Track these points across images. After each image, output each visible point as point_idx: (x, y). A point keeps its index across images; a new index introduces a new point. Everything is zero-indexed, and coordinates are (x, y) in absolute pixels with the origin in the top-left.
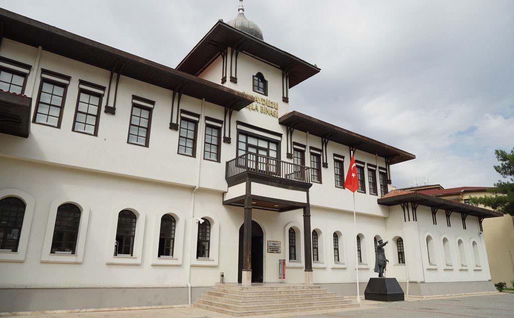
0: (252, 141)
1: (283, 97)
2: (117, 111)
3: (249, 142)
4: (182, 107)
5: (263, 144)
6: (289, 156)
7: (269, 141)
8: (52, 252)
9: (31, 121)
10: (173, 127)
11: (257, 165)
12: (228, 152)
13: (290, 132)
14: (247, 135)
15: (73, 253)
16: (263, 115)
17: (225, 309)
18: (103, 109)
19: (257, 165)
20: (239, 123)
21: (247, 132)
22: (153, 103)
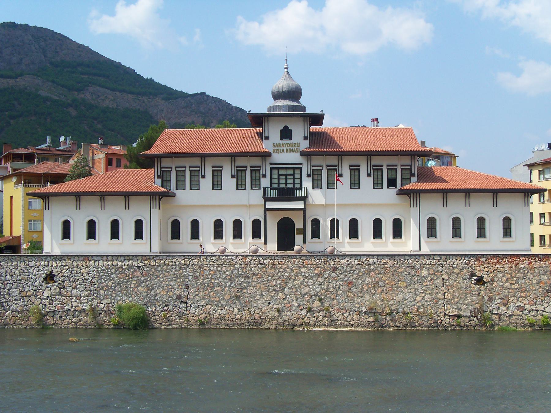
0: (281, 172)
1: (304, 137)
2: (270, 138)
3: (280, 173)
4: (237, 164)
5: (291, 172)
6: (308, 175)
7: (294, 169)
8: (312, 238)
9: (296, 104)
10: (233, 176)
11: (286, 185)
12: (265, 182)
13: (309, 160)
14: (278, 169)
15: (319, 238)
16: (288, 153)
17: (49, 188)
18: (264, 138)
19: (286, 185)
20: (271, 164)
21: (276, 169)
22: (222, 167)
